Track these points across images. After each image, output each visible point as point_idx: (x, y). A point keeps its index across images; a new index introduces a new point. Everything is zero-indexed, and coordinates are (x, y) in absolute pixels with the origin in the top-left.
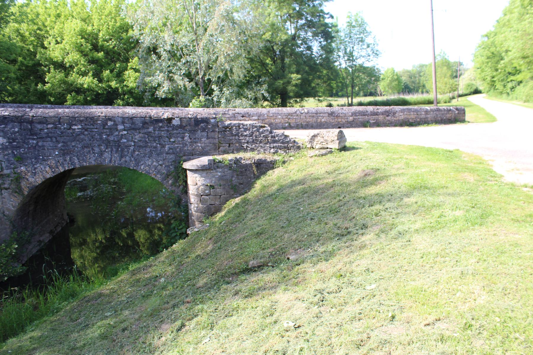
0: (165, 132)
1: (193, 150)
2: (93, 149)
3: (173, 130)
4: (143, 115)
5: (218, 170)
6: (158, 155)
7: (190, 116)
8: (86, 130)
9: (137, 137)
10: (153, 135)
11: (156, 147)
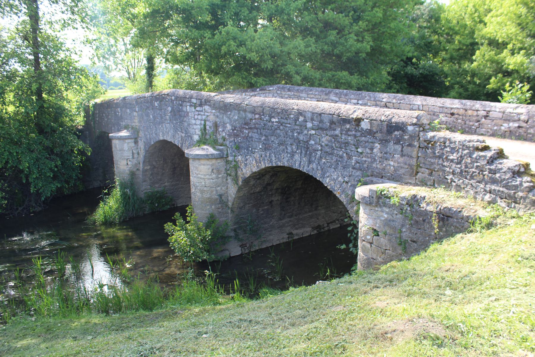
0: (352, 138)
1: (384, 169)
2: (287, 149)
3: (361, 136)
4: (332, 111)
5: (384, 208)
6: (344, 168)
7: (383, 118)
8: (282, 125)
9: (325, 140)
10: (340, 140)
11: (341, 157)
